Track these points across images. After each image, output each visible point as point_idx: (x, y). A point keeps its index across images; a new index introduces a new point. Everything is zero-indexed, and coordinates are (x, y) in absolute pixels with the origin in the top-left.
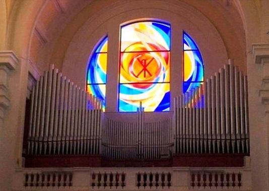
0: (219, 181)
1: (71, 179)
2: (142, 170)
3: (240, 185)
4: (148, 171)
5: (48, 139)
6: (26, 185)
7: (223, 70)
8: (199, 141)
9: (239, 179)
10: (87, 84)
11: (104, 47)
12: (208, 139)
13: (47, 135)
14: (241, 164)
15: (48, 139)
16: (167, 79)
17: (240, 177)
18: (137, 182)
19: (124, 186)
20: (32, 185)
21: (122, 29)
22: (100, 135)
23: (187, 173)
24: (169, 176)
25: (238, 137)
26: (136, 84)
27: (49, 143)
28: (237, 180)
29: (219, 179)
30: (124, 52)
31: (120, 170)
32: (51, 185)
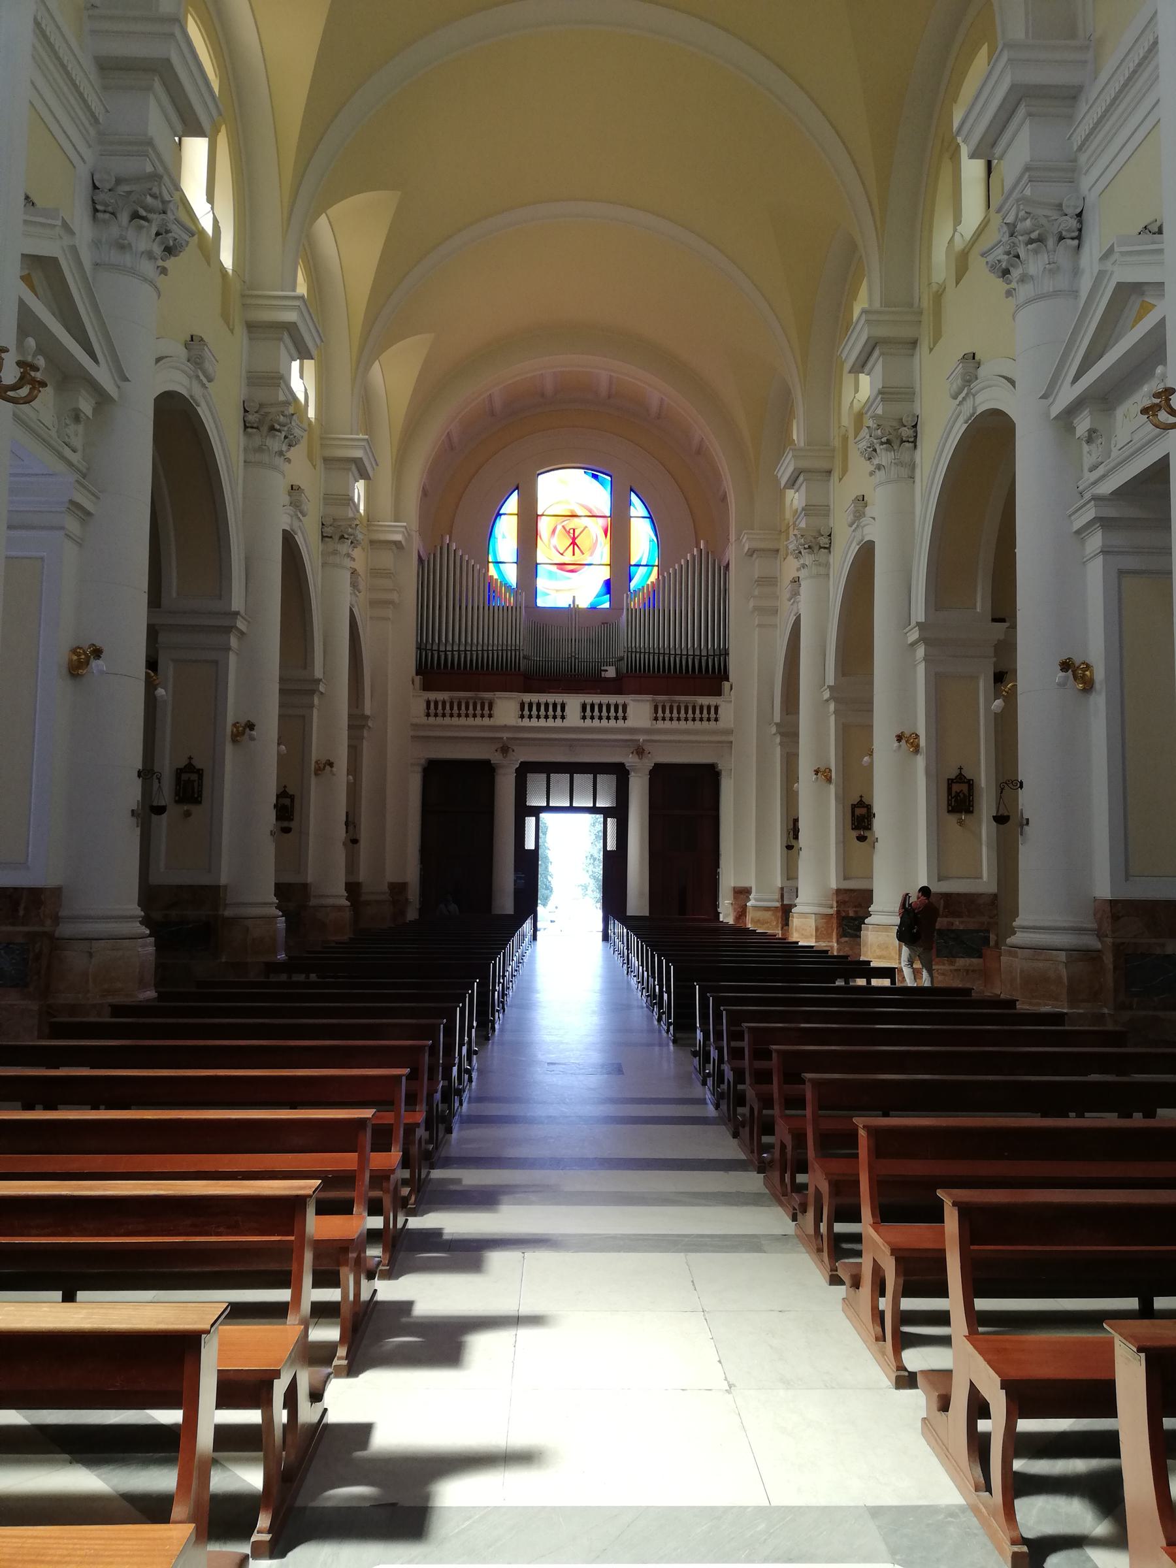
0: (690, 715)
1: (490, 708)
2: (589, 699)
3: (716, 720)
4: (596, 699)
5: (459, 647)
6: (656, 719)
7: (693, 557)
8: (649, 655)
9: (716, 712)
10: (489, 562)
11: (512, 504)
12: (670, 654)
13: (437, 642)
14: (718, 693)
15: (459, 647)
16: (606, 559)
17: (626, 708)
18: (582, 714)
19: (564, 718)
20: (436, 715)
21: (539, 476)
22: (521, 644)
23: (648, 703)
24: (625, 707)
25: (711, 653)
26: (561, 565)
27: (448, 653)
28: (713, 713)
29: (690, 711)
30: (542, 515)
31: (558, 698)
32: (596, 718)
